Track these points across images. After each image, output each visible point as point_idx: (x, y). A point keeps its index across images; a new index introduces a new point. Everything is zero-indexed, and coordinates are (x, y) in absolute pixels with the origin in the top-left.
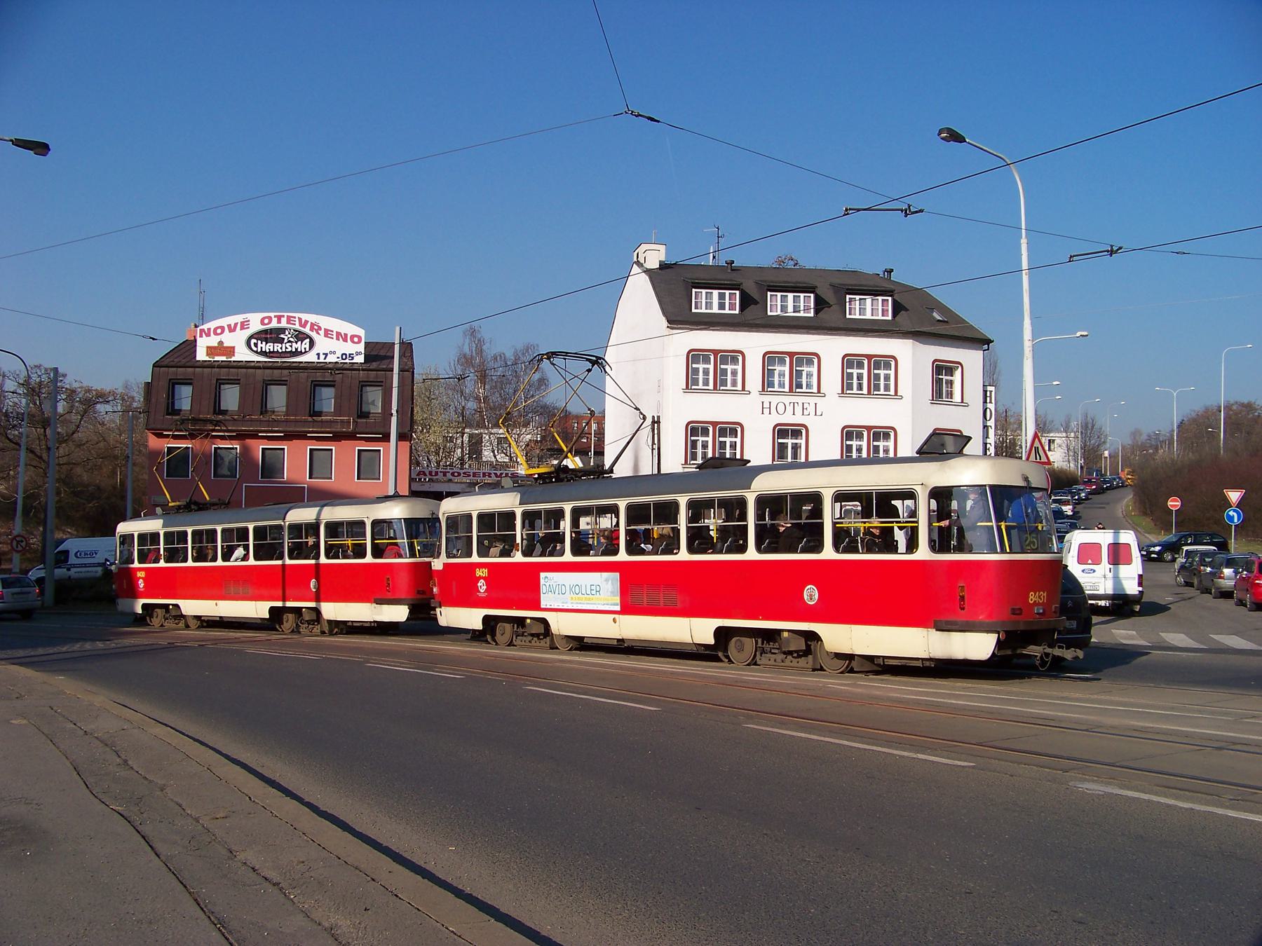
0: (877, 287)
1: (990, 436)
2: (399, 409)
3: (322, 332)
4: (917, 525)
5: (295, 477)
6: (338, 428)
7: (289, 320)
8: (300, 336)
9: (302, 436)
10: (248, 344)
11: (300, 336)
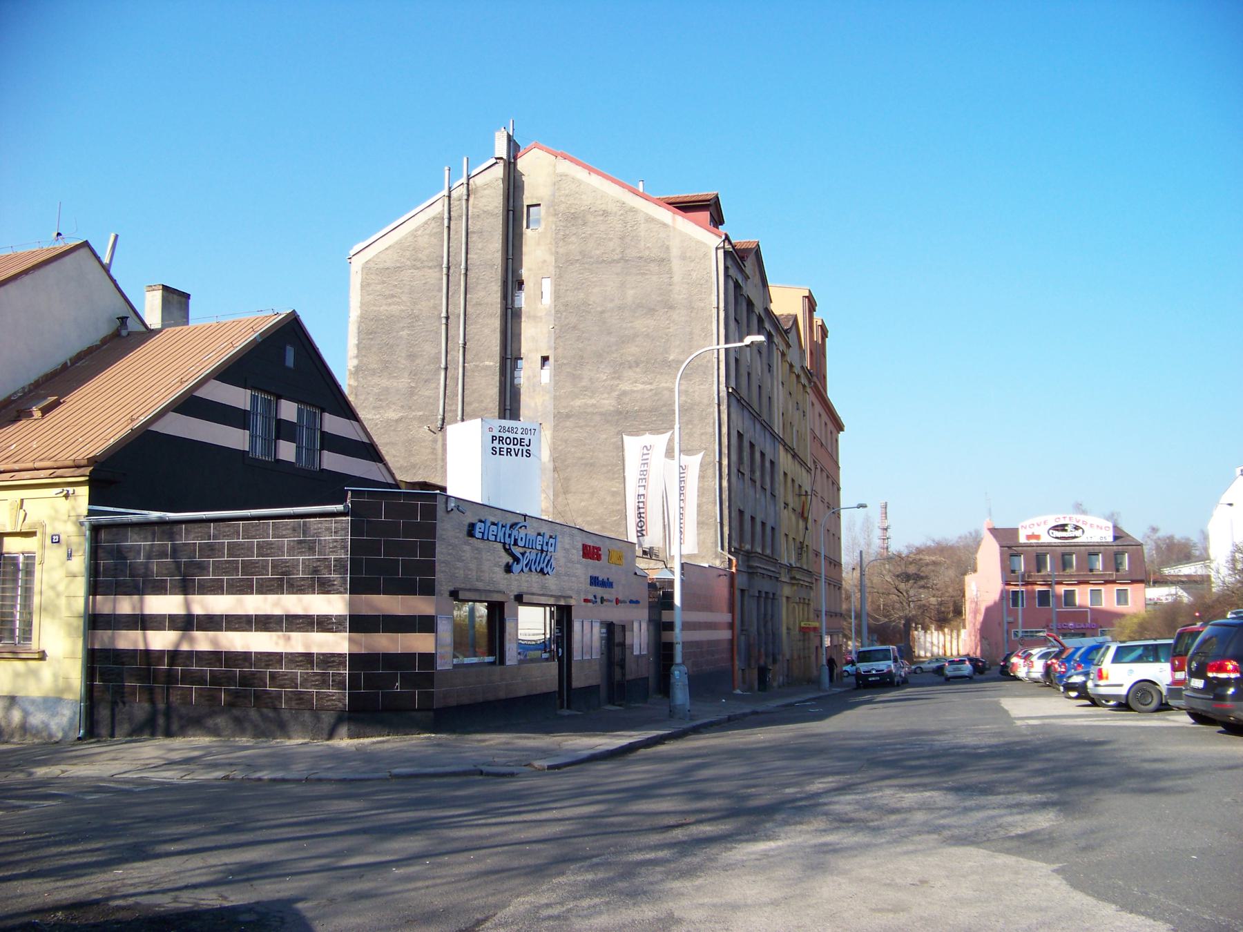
0: (716, 541)
1: (740, 672)
2: (836, 493)
3: (1088, 525)
4: (105, 604)
5: (1083, 603)
6: (1107, 578)
7: (1070, 518)
8: (1076, 528)
9: (1087, 583)
10: (1048, 533)
11: (1076, 528)
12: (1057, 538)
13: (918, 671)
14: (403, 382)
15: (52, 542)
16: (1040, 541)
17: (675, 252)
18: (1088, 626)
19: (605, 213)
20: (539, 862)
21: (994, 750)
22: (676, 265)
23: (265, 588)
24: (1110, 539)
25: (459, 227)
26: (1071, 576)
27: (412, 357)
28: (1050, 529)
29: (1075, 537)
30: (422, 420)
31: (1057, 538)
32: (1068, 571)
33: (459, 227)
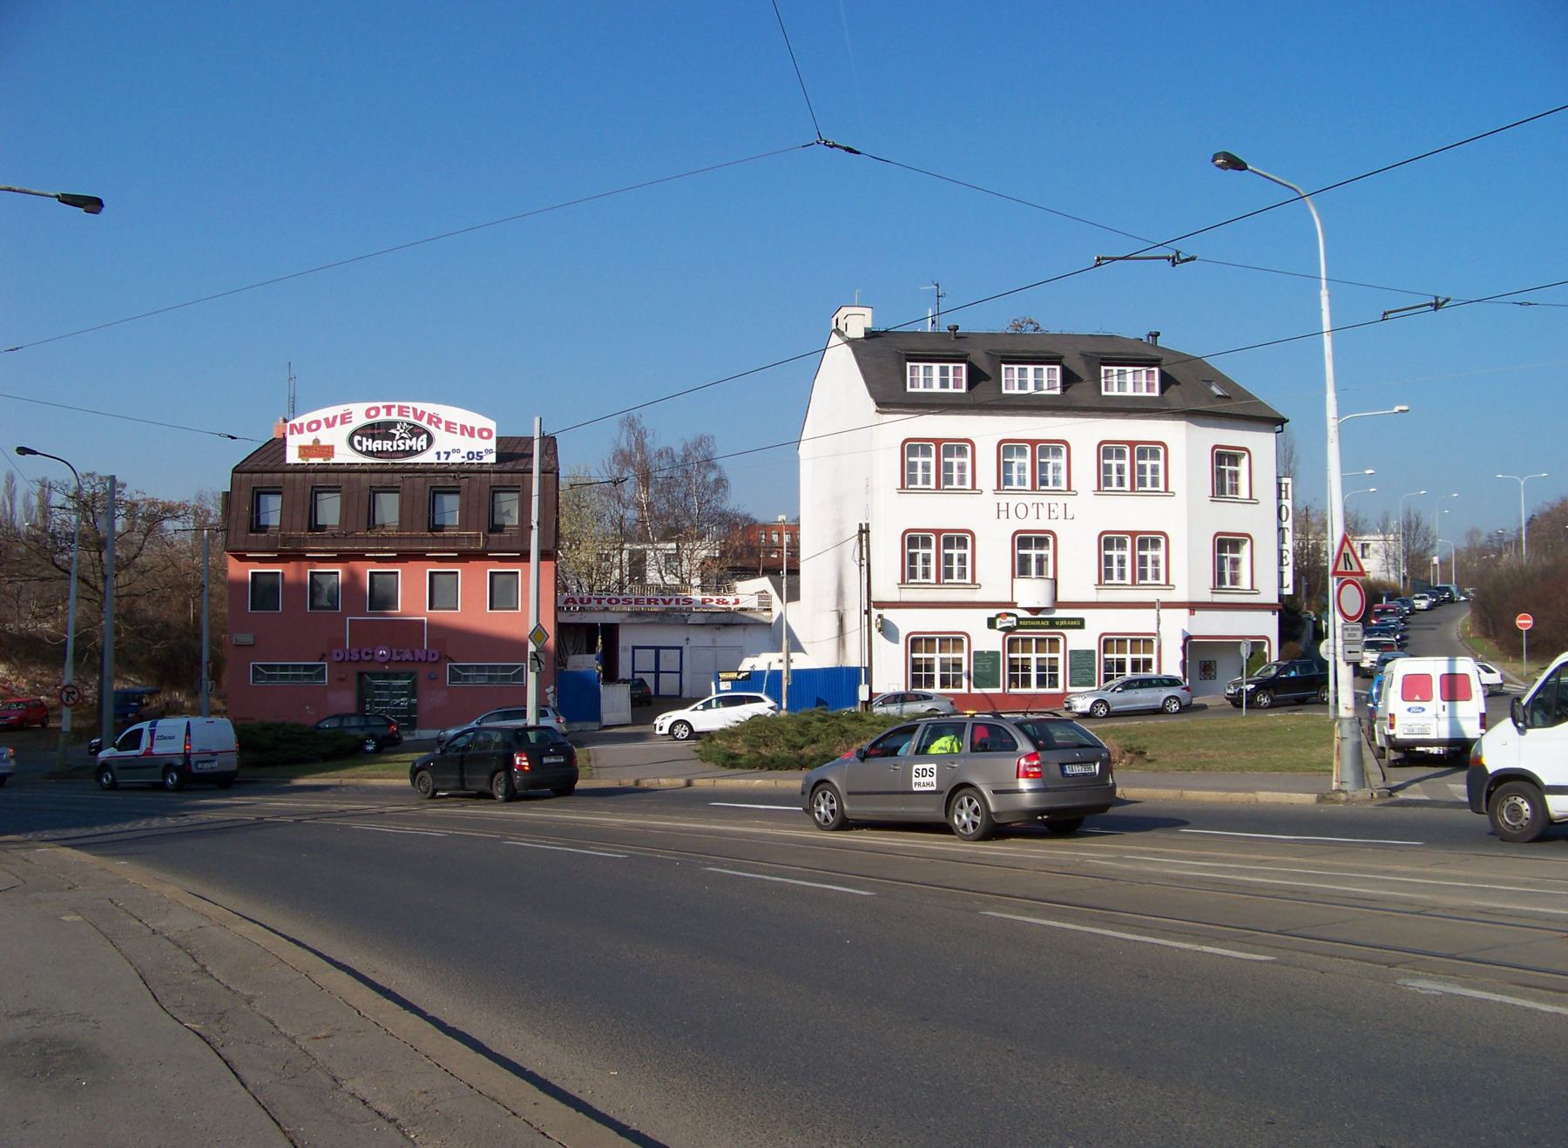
3: (442, 426)
6: (465, 546)
7: (401, 411)
8: (416, 431)
9: (420, 556)
11: (416, 431)
12: (370, 453)
13: (682, 732)
16: (332, 461)
18: (419, 655)
20: (1291, 643)
21: (667, 817)
28: (354, 433)
29: (417, 452)
31: (370, 453)
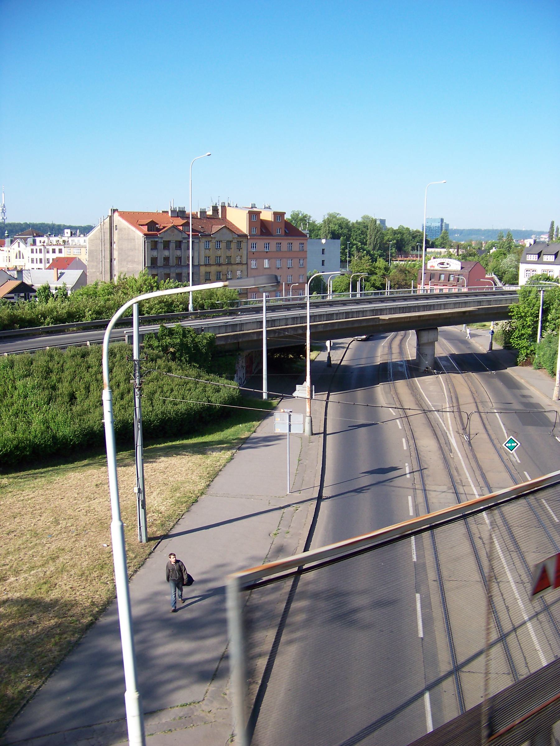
8: (448, 264)
11: (448, 264)
14: (95, 264)
15: (114, 211)
17: (136, 237)
19: (125, 229)
22: (136, 241)
23: (537, 331)
24: (460, 269)
25: (103, 231)
26: (441, 283)
27: (96, 258)
30: (98, 272)
32: (440, 281)
33: (103, 231)
